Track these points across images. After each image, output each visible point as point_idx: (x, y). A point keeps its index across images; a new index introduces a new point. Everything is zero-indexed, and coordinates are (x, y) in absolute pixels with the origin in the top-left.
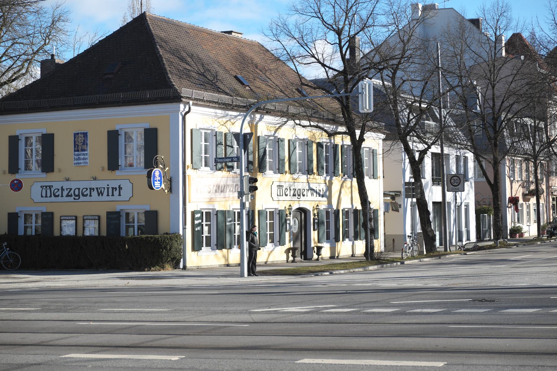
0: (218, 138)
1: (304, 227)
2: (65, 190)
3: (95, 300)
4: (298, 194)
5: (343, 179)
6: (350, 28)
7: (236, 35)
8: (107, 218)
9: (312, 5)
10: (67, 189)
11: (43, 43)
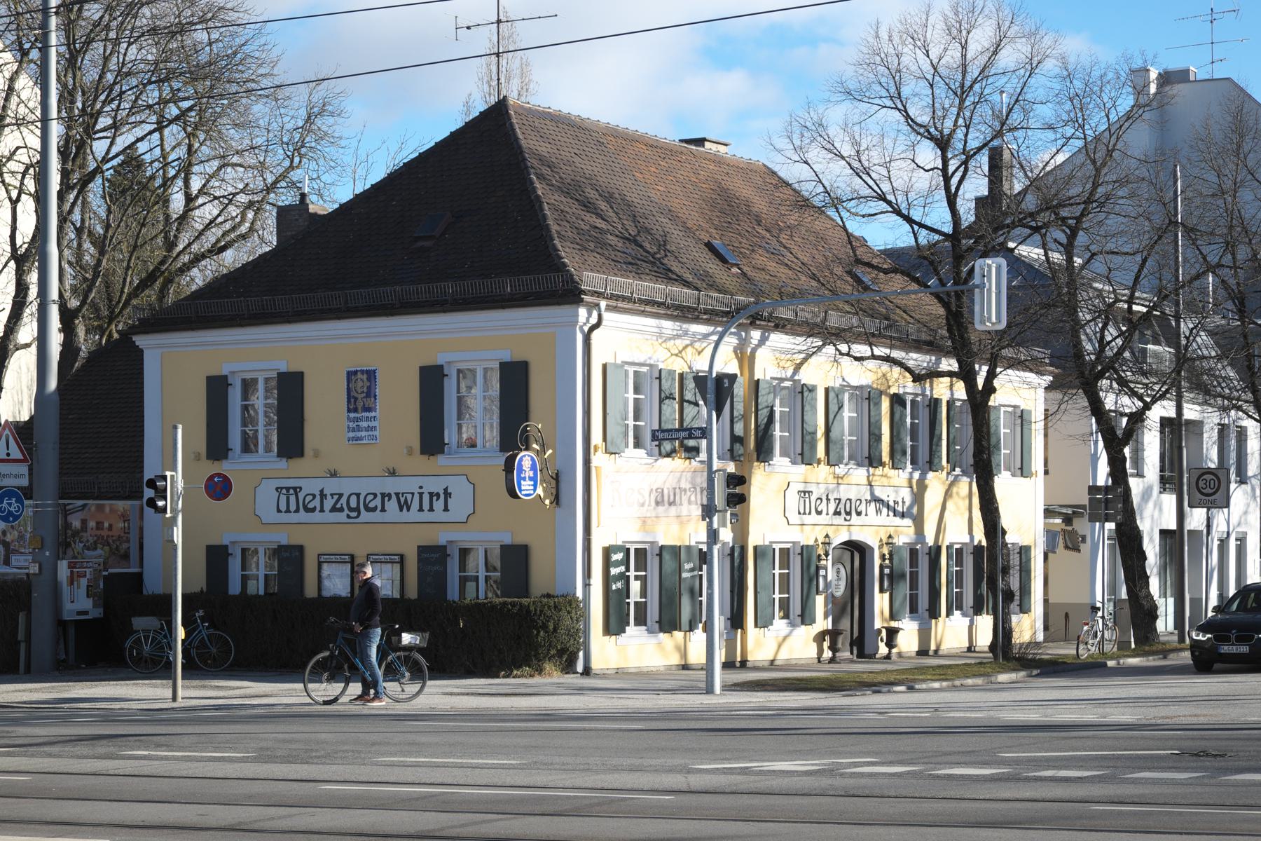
0: (665, 385)
1: (859, 587)
2: (329, 497)
3: (374, 737)
4: (846, 510)
5: (951, 478)
6: (966, 135)
7: (714, 147)
8: (419, 560)
9: (883, 80)
10: (332, 495)
11: (287, 163)
